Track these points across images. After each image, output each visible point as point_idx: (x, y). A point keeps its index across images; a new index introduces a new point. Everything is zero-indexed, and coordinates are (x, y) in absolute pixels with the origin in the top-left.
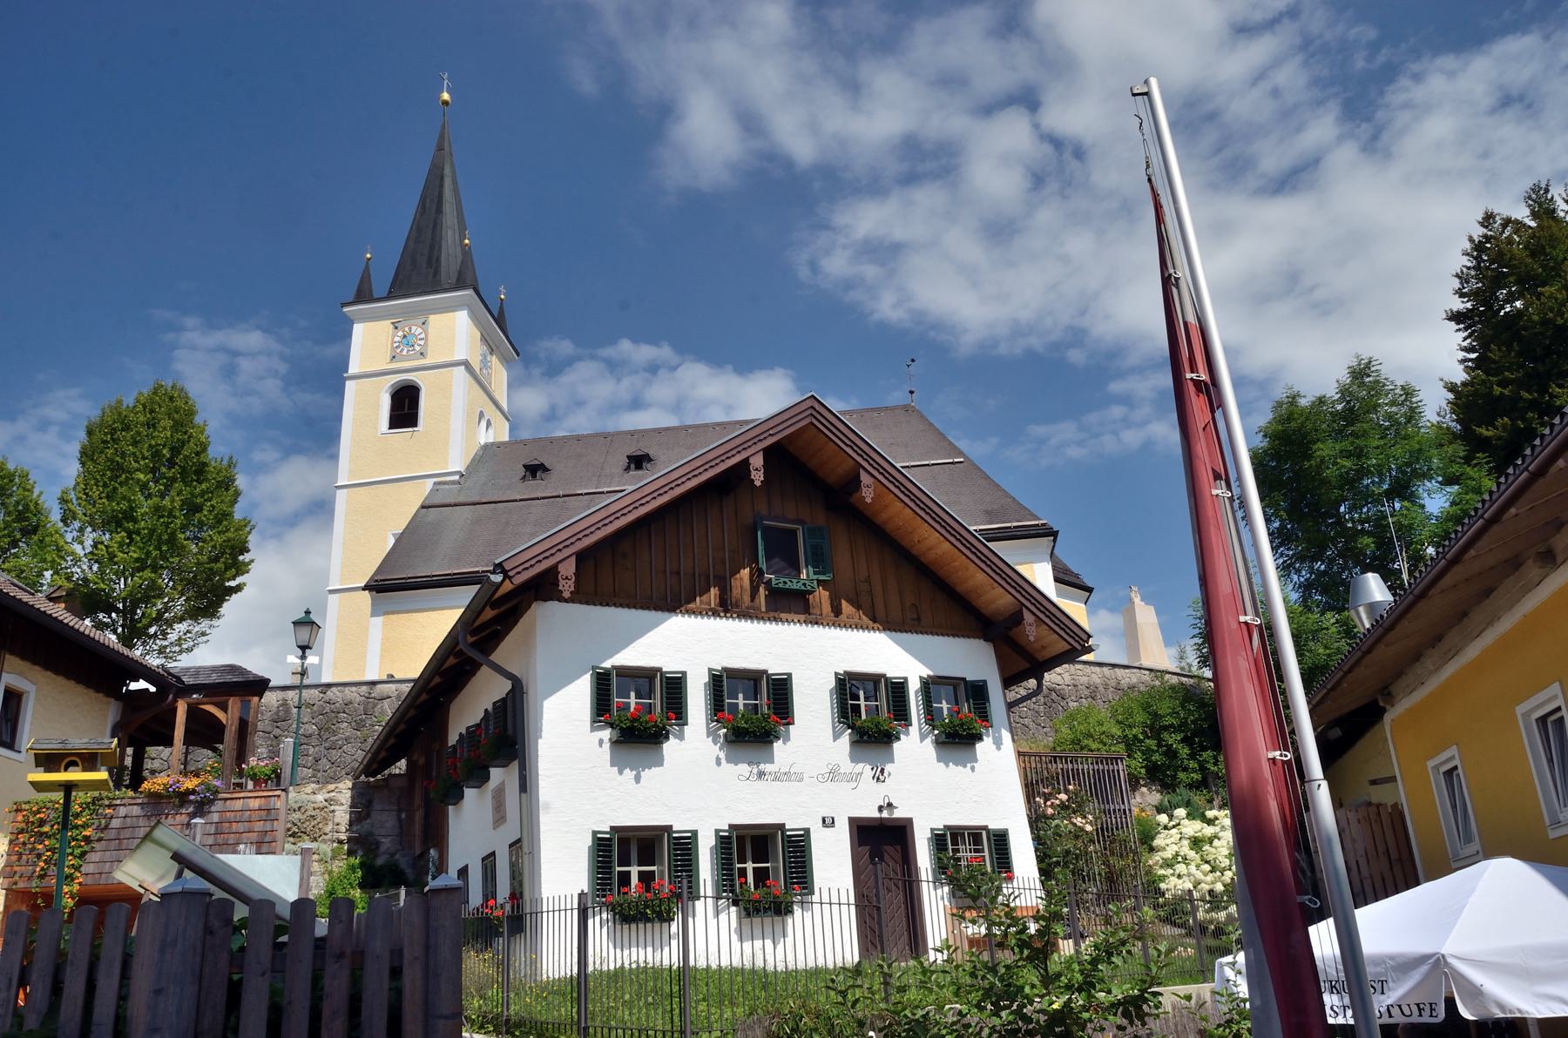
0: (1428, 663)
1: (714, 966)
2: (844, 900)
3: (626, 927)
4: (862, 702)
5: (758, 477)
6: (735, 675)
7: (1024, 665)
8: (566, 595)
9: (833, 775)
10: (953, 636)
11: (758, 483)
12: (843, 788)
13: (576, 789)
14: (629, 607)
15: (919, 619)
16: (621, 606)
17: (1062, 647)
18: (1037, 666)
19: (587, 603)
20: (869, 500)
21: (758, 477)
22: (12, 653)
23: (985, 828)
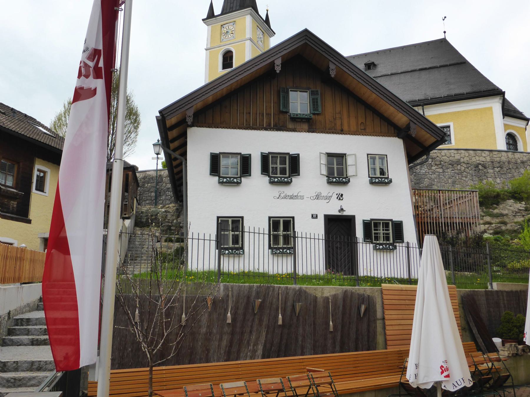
0: (225, 92)
1: (383, 278)
2: (195, 242)
3: (276, 258)
4: (335, 166)
5: (278, 69)
6: (275, 155)
7: (420, 149)
8: (189, 123)
9: (318, 197)
10: (382, 136)
11: (278, 72)
12: (322, 203)
13: (206, 202)
14: (227, 128)
15: (365, 129)
16: (223, 128)
17: (433, 140)
18: (426, 150)
19: (209, 127)
20: (333, 76)
21: (278, 69)
22: (39, 158)
23: (391, 220)
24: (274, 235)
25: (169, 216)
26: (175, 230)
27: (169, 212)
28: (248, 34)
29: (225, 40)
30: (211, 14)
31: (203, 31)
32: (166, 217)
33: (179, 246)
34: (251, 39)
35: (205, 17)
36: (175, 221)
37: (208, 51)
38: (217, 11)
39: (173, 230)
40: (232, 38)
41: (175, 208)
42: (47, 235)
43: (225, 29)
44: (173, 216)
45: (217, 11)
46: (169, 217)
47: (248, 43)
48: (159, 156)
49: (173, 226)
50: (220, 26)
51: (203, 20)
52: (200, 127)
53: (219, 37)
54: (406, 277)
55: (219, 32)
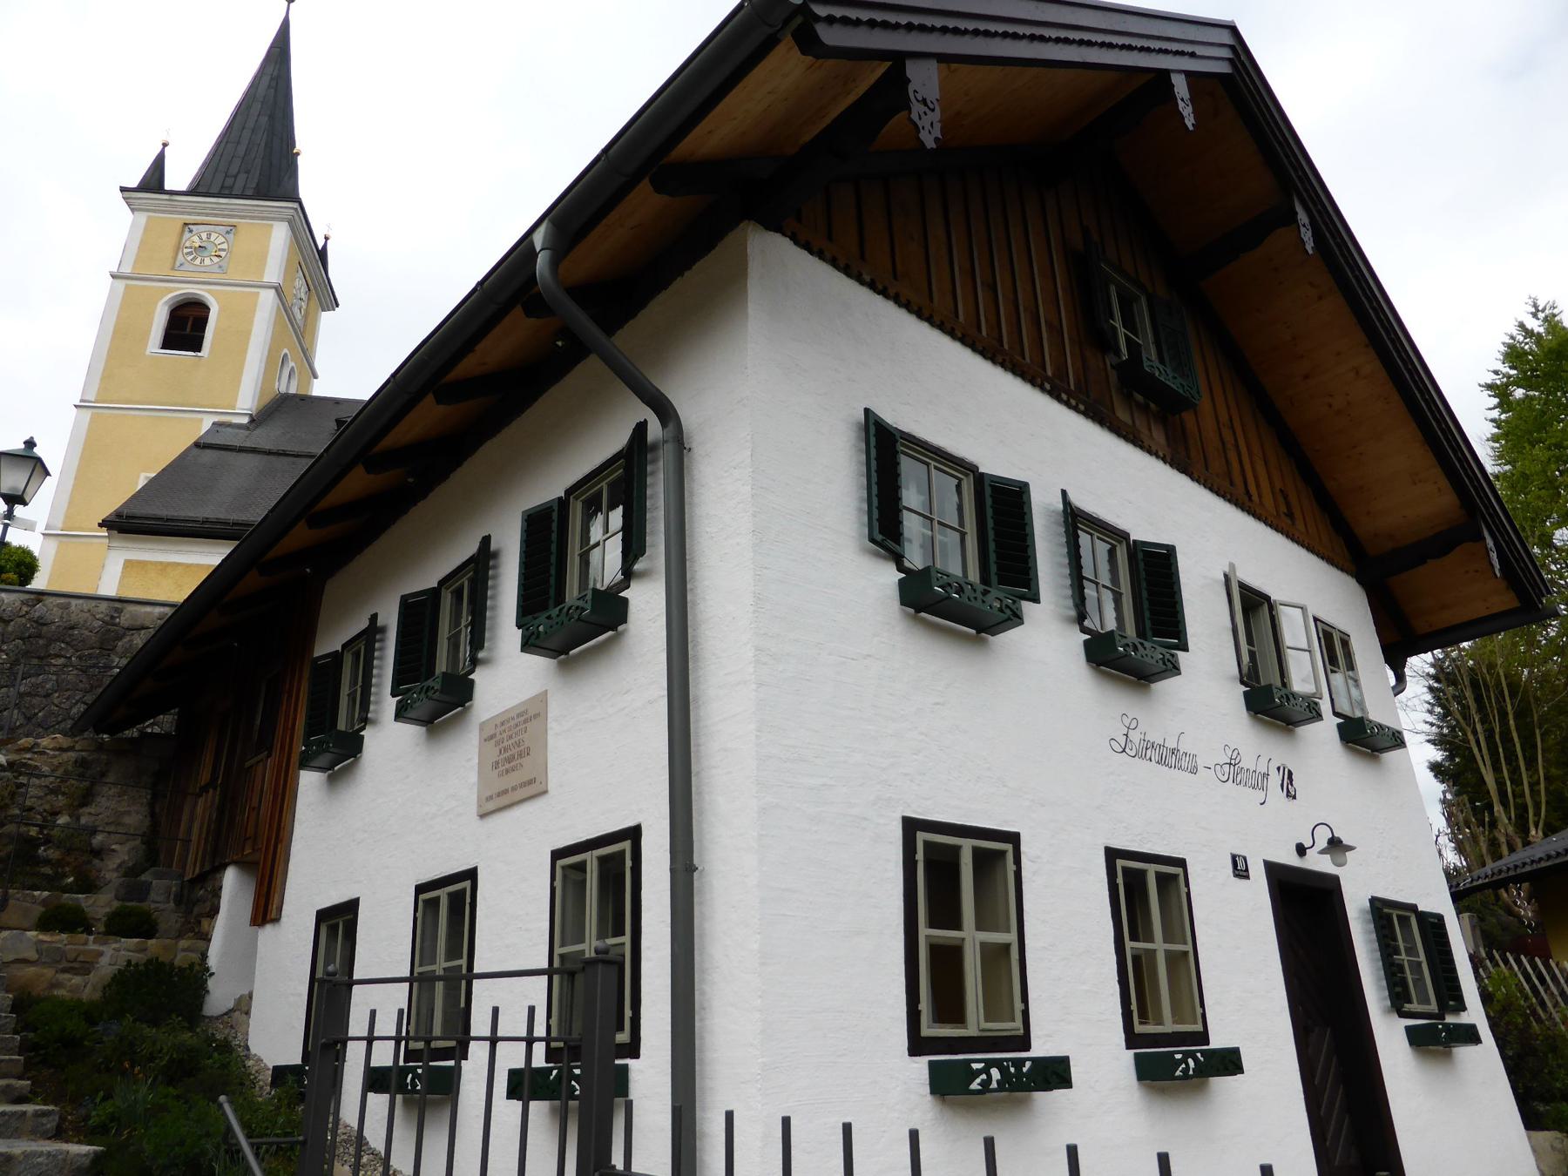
24: (936, 950)
25: (32, 791)
26: (60, 863)
27: (34, 772)
28: (273, 272)
29: (187, 267)
30: (154, 181)
31: (118, 226)
32: (13, 795)
33: (137, 957)
34: (278, 290)
35: (134, 183)
36: (63, 820)
37: (121, 284)
38: (179, 177)
39: (47, 862)
40: (216, 269)
41: (72, 755)
42: (326, 318)
43: (196, 238)
44: (54, 791)
45: (179, 177)
46: (34, 790)
47: (268, 298)
48: (19, 510)
49: (48, 841)
50: (180, 225)
51: (123, 189)
52: (807, 247)
53: (170, 254)
54: (358, 974)
55: (173, 239)
